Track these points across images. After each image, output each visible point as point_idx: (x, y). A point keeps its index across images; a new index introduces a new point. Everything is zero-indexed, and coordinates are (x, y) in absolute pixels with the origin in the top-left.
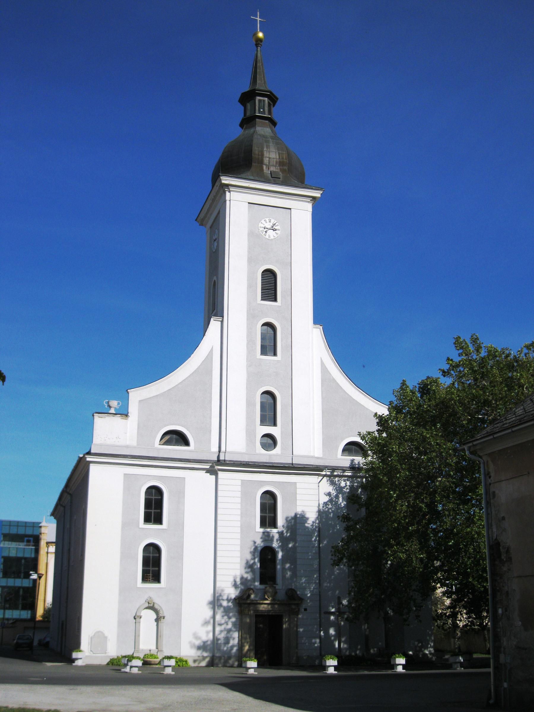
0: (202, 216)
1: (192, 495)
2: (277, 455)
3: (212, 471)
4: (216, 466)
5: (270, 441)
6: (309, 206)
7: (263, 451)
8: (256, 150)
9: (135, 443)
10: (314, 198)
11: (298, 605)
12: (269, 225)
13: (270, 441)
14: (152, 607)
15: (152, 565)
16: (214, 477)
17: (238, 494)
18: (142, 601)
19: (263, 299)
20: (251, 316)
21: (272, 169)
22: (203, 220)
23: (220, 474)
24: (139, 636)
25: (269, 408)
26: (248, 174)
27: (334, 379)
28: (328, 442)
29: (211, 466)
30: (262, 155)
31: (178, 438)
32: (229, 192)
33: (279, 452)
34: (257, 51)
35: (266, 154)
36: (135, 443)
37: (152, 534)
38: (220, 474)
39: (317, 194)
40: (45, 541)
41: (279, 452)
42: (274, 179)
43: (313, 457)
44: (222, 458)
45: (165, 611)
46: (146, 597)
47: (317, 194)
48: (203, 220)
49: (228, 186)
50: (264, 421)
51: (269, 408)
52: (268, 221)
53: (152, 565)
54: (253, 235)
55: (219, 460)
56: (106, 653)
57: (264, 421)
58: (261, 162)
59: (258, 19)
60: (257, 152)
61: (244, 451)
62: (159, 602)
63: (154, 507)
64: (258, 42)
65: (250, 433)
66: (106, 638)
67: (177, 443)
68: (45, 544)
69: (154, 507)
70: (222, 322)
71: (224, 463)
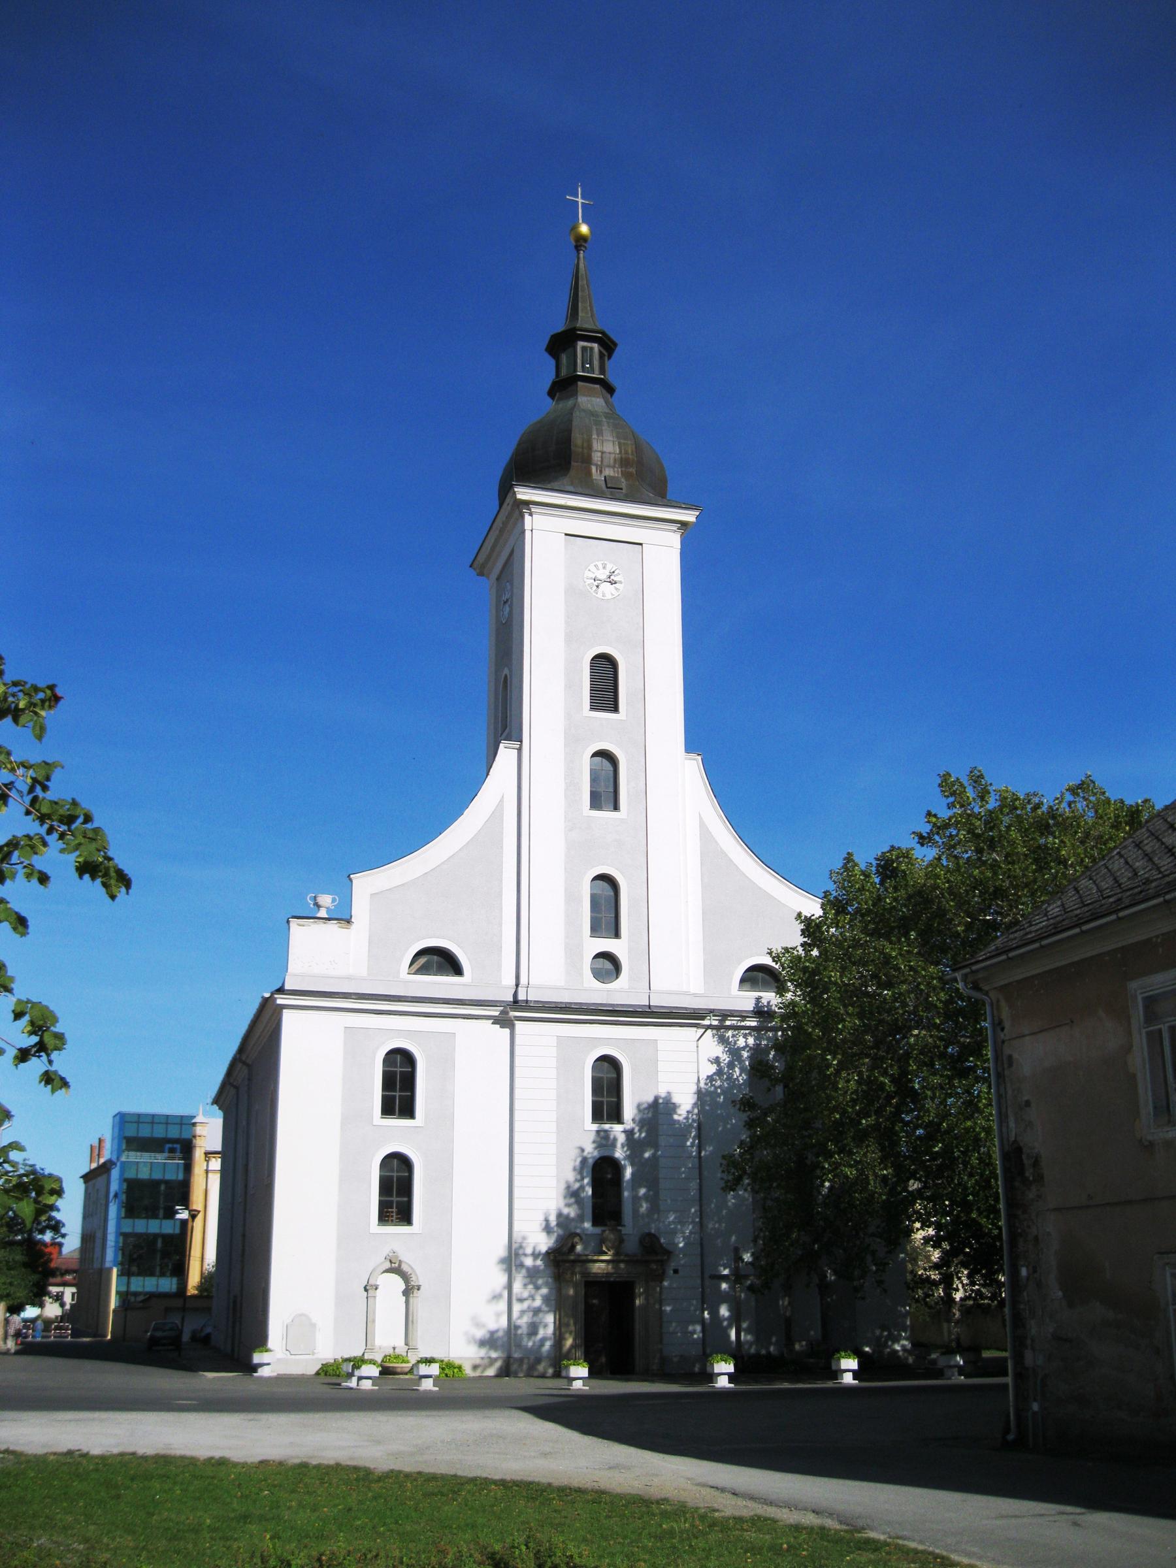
0: (481, 558)
1: (465, 1063)
2: (620, 992)
3: (504, 1021)
4: (512, 1011)
5: (608, 965)
6: (674, 539)
7: (597, 984)
8: (577, 439)
9: (364, 972)
10: (683, 525)
11: (663, 1263)
12: (602, 574)
13: (608, 965)
14: (396, 1269)
15: (396, 1193)
16: (507, 1031)
17: (556, 1062)
18: (378, 1260)
19: (592, 708)
20: (572, 739)
21: (608, 472)
22: (483, 566)
23: (519, 1025)
24: (374, 1321)
25: (606, 905)
26: (565, 482)
27: (723, 852)
28: (713, 966)
29: (502, 1012)
30: (590, 447)
31: (441, 961)
32: (531, 514)
33: (626, 986)
34: (578, 258)
35: (596, 446)
36: (364, 972)
37: (397, 1135)
38: (519, 1025)
39: (690, 516)
40: (203, 1151)
41: (626, 986)
42: (611, 491)
43: (686, 994)
44: (521, 997)
45: (421, 1276)
46: (386, 1251)
47: (690, 516)
48: (483, 566)
49: (527, 503)
50: (596, 929)
51: (606, 905)
52: (601, 567)
53: (396, 1193)
54: (573, 593)
55: (516, 1001)
56: (313, 1354)
57: (596, 929)
58: (587, 460)
59: (580, 200)
60: (579, 442)
61: (562, 983)
62: (411, 1260)
63: (399, 1087)
64: (581, 241)
65: (572, 951)
66: (313, 1326)
67: (440, 971)
68: (203, 1156)
69: (399, 1087)
70: (520, 750)
71: (527, 1006)
